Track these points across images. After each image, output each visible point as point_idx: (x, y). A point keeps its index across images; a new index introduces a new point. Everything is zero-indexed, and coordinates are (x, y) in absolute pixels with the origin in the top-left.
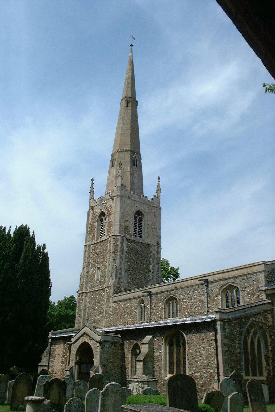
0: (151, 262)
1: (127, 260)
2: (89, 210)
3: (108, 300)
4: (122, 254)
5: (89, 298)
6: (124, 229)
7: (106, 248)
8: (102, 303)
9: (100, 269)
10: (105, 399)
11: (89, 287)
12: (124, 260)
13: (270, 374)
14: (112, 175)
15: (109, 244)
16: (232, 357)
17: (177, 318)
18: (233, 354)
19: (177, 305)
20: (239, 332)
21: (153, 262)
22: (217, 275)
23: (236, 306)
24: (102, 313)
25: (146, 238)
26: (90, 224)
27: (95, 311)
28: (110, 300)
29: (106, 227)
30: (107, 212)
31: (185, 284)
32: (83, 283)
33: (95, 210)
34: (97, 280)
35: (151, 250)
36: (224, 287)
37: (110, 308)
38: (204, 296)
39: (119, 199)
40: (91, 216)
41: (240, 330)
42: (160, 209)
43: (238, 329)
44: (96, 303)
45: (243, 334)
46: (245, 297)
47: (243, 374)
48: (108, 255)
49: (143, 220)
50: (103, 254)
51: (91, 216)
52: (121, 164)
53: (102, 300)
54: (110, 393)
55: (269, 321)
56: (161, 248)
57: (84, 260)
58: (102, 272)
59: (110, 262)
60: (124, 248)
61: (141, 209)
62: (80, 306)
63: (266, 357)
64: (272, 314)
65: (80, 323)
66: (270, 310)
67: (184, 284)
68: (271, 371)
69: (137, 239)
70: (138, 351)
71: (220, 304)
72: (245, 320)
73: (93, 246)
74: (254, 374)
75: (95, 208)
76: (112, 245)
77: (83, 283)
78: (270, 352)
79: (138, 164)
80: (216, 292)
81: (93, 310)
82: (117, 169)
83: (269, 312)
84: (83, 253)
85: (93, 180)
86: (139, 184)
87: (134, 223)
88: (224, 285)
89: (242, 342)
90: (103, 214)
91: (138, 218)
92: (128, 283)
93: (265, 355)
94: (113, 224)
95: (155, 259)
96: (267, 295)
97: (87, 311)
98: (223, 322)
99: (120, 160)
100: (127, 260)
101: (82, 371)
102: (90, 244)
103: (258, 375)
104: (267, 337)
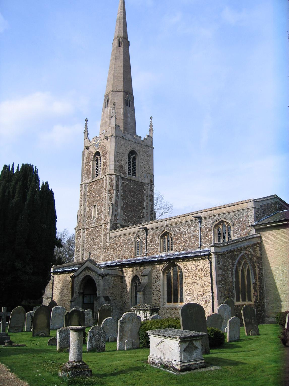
1: (122, 198)
2: (84, 150)
3: (105, 236)
5: (87, 234)
6: (119, 168)
7: (102, 187)
8: (99, 238)
10: (123, 326)
11: (86, 224)
12: (119, 198)
13: (257, 299)
14: (106, 116)
15: (104, 183)
17: (172, 251)
21: (147, 199)
22: (210, 212)
23: (227, 241)
24: (99, 248)
25: (140, 177)
26: (85, 164)
29: (102, 167)
30: (102, 152)
32: (80, 220)
33: (90, 150)
34: (94, 217)
35: (145, 187)
36: (216, 223)
37: (107, 243)
38: (198, 231)
39: (113, 139)
40: (86, 156)
43: (231, 261)
45: (235, 266)
47: (235, 300)
48: (104, 193)
49: (137, 159)
50: (99, 192)
51: (86, 156)
52: (115, 105)
54: (127, 321)
56: (154, 186)
57: (81, 198)
58: (98, 210)
60: (119, 187)
61: (135, 149)
62: (78, 242)
63: (254, 284)
65: (79, 257)
66: (258, 243)
67: (178, 220)
68: (258, 296)
70: (137, 282)
71: (213, 239)
72: (237, 252)
73: (89, 185)
74: (244, 300)
76: (108, 184)
77: (80, 220)
78: (258, 281)
79: (131, 105)
80: (209, 227)
82: (110, 110)
83: (258, 245)
84: (80, 191)
85: (87, 120)
86: (132, 124)
88: (217, 221)
89: (234, 273)
90: (98, 153)
91: (132, 157)
92: (123, 219)
94: (108, 163)
96: (255, 229)
97: (85, 247)
99: (113, 101)
100: (122, 198)
101: (85, 301)
102: (86, 183)
103: (247, 301)
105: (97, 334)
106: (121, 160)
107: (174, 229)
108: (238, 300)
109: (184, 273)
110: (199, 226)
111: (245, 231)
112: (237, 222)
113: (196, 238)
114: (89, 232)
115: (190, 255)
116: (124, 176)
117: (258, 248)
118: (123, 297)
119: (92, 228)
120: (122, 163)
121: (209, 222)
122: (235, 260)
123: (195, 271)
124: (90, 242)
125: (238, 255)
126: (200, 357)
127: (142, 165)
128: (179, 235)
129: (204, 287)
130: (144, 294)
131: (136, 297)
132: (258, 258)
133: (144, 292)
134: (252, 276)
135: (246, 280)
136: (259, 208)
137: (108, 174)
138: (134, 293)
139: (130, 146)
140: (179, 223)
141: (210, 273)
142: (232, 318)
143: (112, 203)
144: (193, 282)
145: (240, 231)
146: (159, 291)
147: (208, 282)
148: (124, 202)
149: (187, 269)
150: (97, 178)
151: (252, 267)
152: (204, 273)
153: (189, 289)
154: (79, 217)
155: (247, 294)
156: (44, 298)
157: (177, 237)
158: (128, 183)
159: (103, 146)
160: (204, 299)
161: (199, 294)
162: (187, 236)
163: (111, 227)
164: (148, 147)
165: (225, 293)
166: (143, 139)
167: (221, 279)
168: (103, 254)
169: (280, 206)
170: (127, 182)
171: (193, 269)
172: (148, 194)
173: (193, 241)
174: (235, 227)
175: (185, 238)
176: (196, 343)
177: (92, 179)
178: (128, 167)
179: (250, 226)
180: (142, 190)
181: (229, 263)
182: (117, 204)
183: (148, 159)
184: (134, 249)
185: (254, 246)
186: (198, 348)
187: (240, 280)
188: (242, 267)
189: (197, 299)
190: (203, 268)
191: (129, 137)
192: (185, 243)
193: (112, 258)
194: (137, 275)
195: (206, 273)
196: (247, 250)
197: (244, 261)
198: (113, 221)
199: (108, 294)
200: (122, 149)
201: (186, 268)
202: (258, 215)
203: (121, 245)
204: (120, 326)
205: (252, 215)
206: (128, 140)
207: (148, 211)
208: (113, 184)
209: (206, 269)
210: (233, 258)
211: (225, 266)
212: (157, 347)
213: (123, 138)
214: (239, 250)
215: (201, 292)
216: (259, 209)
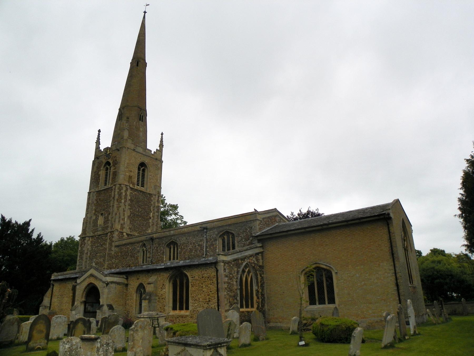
0: (152, 210)
1: (130, 207)
4: (125, 201)
7: (110, 196)
9: (103, 215)
11: (91, 232)
12: (127, 207)
13: (259, 306)
16: (231, 293)
18: (231, 290)
19: (177, 249)
20: (236, 271)
21: (154, 210)
27: (97, 255)
28: (113, 244)
31: (186, 230)
35: (152, 198)
36: (221, 233)
37: (112, 252)
40: (96, 165)
41: (237, 269)
42: (162, 162)
43: (236, 269)
44: (98, 247)
45: (240, 273)
46: (239, 242)
48: (112, 202)
49: (146, 171)
53: (104, 244)
55: (260, 262)
58: (105, 218)
60: (127, 197)
63: (256, 292)
64: (262, 256)
65: (82, 265)
68: (260, 303)
69: (139, 188)
72: (241, 261)
74: (247, 307)
75: (100, 157)
76: (116, 193)
78: (260, 288)
81: (96, 253)
87: (138, 174)
88: (221, 232)
89: (239, 280)
91: (142, 169)
92: (130, 229)
93: (256, 291)
95: (156, 207)
98: (224, 264)
100: (130, 207)
104: (257, 275)
105: (105, 344)
106: (131, 171)
107: (180, 238)
109: (190, 281)
111: (249, 241)
112: (241, 232)
114: (94, 239)
116: (133, 186)
117: (260, 257)
118: (127, 305)
119: (98, 236)
120: (132, 174)
121: (214, 232)
122: (239, 268)
127: (150, 177)
128: (185, 245)
129: (210, 294)
131: (141, 305)
132: (260, 266)
133: (150, 301)
135: (249, 288)
138: (138, 301)
139: (141, 158)
140: (185, 233)
141: (216, 281)
144: (199, 289)
146: (164, 299)
147: (214, 289)
148: (131, 212)
149: (194, 277)
150: (106, 187)
151: (255, 275)
152: (211, 281)
155: (250, 301)
158: (136, 193)
160: (210, 306)
161: (205, 301)
162: (192, 245)
164: (157, 161)
165: (230, 301)
166: (153, 153)
167: (226, 287)
168: (108, 263)
169: (279, 219)
170: (135, 192)
171: (200, 277)
172: (155, 205)
173: (199, 250)
175: (190, 247)
176: (221, 350)
179: (253, 237)
182: (124, 213)
183: (157, 171)
185: (257, 255)
187: (244, 288)
188: (246, 275)
190: (210, 276)
191: (140, 150)
192: (191, 252)
194: (142, 282)
195: (213, 281)
197: (247, 269)
199: (111, 303)
200: (133, 161)
201: (192, 276)
202: (260, 226)
206: (139, 153)
209: (212, 277)
210: (238, 266)
211: (231, 274)
213: (134, 150)
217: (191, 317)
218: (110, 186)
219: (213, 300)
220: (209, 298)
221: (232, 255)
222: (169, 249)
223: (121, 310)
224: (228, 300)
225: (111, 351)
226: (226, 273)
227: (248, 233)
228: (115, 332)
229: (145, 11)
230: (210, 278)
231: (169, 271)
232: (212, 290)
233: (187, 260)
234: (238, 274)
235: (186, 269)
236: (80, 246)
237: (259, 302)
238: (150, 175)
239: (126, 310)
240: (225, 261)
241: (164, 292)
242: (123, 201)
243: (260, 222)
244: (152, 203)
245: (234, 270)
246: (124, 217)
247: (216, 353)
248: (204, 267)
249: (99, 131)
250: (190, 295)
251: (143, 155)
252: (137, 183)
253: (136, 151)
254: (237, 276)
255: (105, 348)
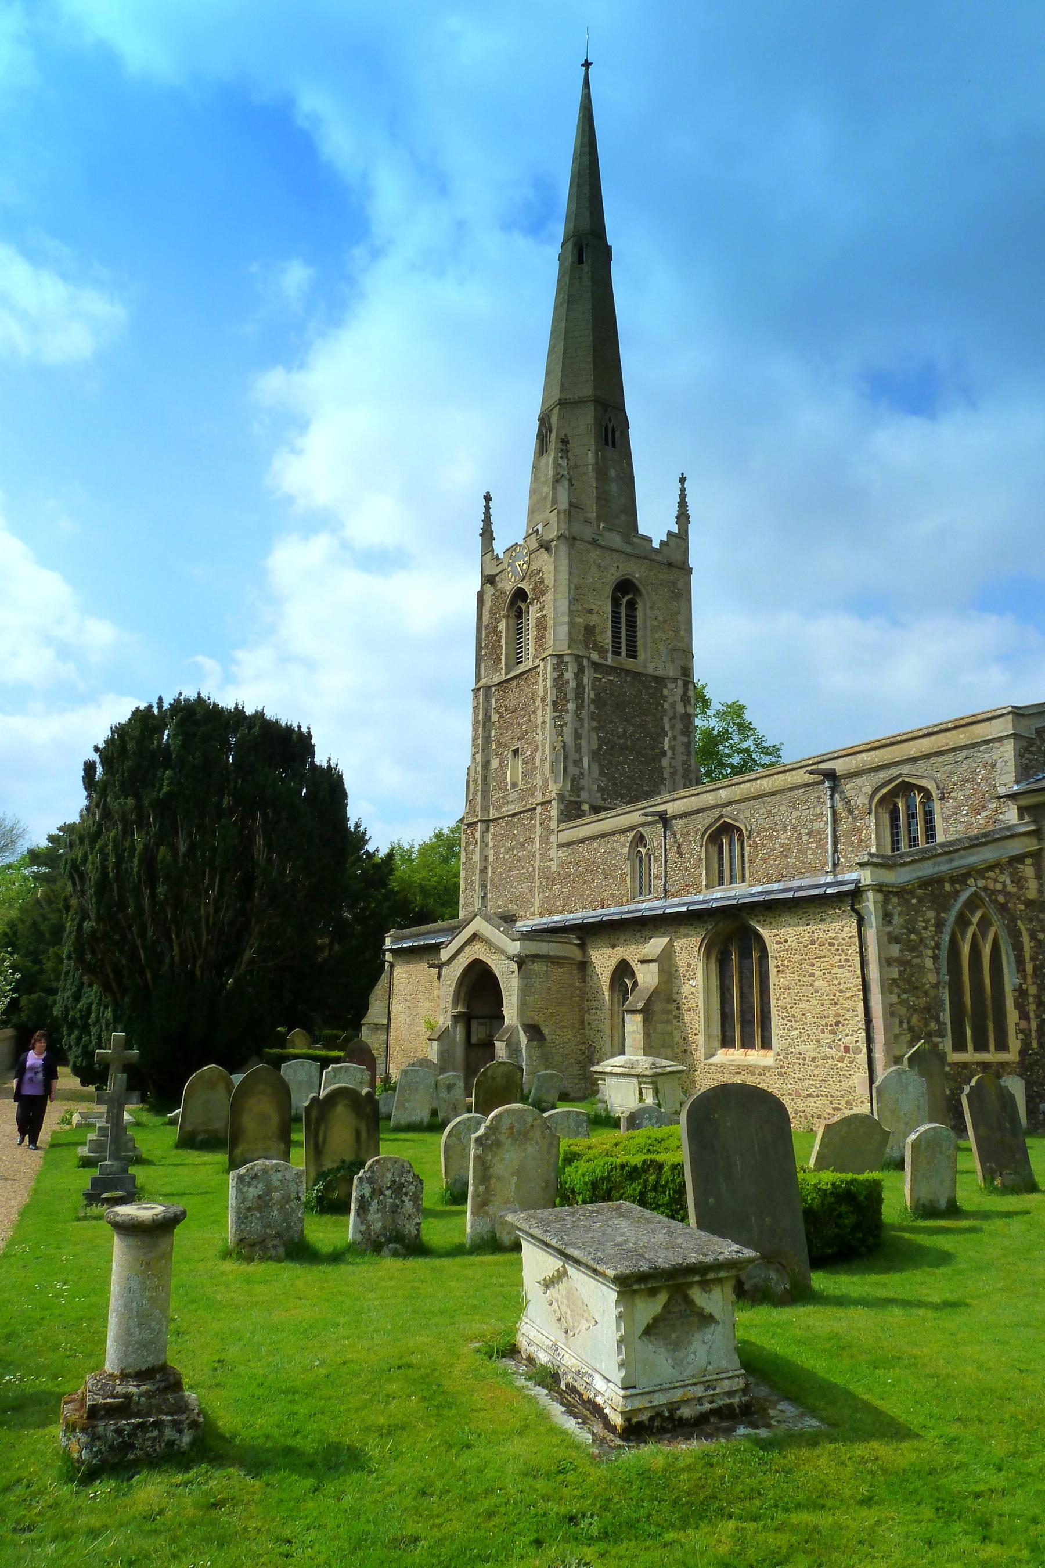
0: (667, 727)
1: (595, 724)
3: (545, 840)
4: (579, 707)
7: (534, 693)
8: (530, 847)
12: (586, 725)
14: (543, 479)
18: (917, 988)
21: (672, 727)
26: (486, 628)
29: (533, 634)
30: (533, 590)
32: (475, 794)
34: (514, 785)
35: (665, 692)
36: (884, 791)
40: (488, 604)
41: (938, 915)
45: (948, 930)
46: (950, 817)
48: (539, 712)
49: (639, 606)
50: (524, 709)
51: (488, 604)
54: (502, 1138)
57: (475, 730)
59: (547, 733)
63: (1017, 994)
64: (1037, 866)
67: (761, 785)
68: (1034, 1034)
74: (981, 1046)
77: (475, 794)
78: (1029, 980)
80: (861, 806)
82: (555, 459)
83: (1028, 861)
84: (471, 710)
89: (944, 954)
91: (624, 601)
92: (601, 789)
98: (885, 896)
102: (490, 683)
103: (992, 1047)
104: (1020, 934)
105: (388, 1188)
106: (590, 611)
108: (959, 1045)
110: (829, 801)
113: (820, 839)
115: (792, 893)
118: (587, 1027)
120: (594, 620)
121: (860, 788)
122: (946, 909)
123: (810, 946)
124: (504, 857)
125: (956, 894)
126: (724, 1364)
127: (656, 623)
129: (838, 1000)
130: (646, 1021)
134: (1009, 963)
135: (987, 980)
136: (1034, 736)
137: (550, 652)
139: (618, 567)
142: (922, 1129)
143: (562, 741)
145: (966, 814)
147: (852, 983)
148: (599, 738)
149: (782, 940)
150: (521, 669)
152: (840, 955)
153: (791, 1008)
154: (472, 787)
155: (991, 1026)
156: (364, 1028)
157: (757, 839)
158: (611, 678)
159: (535, 572)
161: (824, 1023)
163: (561, 813)
166: (656, 545)
167: (896, 976)
173: (811, 849)
174: (948, 802)
175: (783, 841)
177: (506, 674)
178: (613, 631)
179: (999, 797)
180: (658, 698)
181: (926, 921)
182: (580, 744)
184: (628, 878)
185: (1015, 864)
186: (717, 1323)
188: (974, 935)
189: (818, 1041)
192: (786, 856)
193: (564, 906)
195: (847, 955)
196: (989, 878)
197: (978, 915)
198: (567, 794)
199: (537, 1019)
203: (591, 868)
204: (477, 1157)
205: (1006, 762)
207: (678, 763)
208: (567, 681)
210: (941, 903)
211: (912, 931)
212: (545, 1293)
213: (594, 542)
214: (960, 878)
215: (828, 1017)
216: (1031, 742)
217: (780, 1074)
218: (530, 665)
219: (851, 1022)
220: (837, 1015)
221: (916, 866)
222: (716, 848)
223: (567, 1041)
224: (905, 1021)
225: (410, 1212)
226: (891, 929)
227: (982, 785)
228: (460, 1133)
229: (586, 61)
230: (836, 947)
231: (705, 922)
232: (846, 986)
233: (774, 882)
234: (942, 932)
235: (756, 916)
236: (465, 850)
237: (1027, 1032)
238: (654, 617)
239: (584, 1043)
240: (887, 885)
241: (693, 990)
242: (571, 706)
243: (1025, 744)
244: (666, 706)
245: (923, 916)
246: (580, 754)
247: (683, 1307)
248: (815, 907)
249: (488, 498)
250: (773, 1003)
251: (623, 555)
252: (613, 647)
253: (599, 546)
254: (936, 938)
255: (388, 1200)
